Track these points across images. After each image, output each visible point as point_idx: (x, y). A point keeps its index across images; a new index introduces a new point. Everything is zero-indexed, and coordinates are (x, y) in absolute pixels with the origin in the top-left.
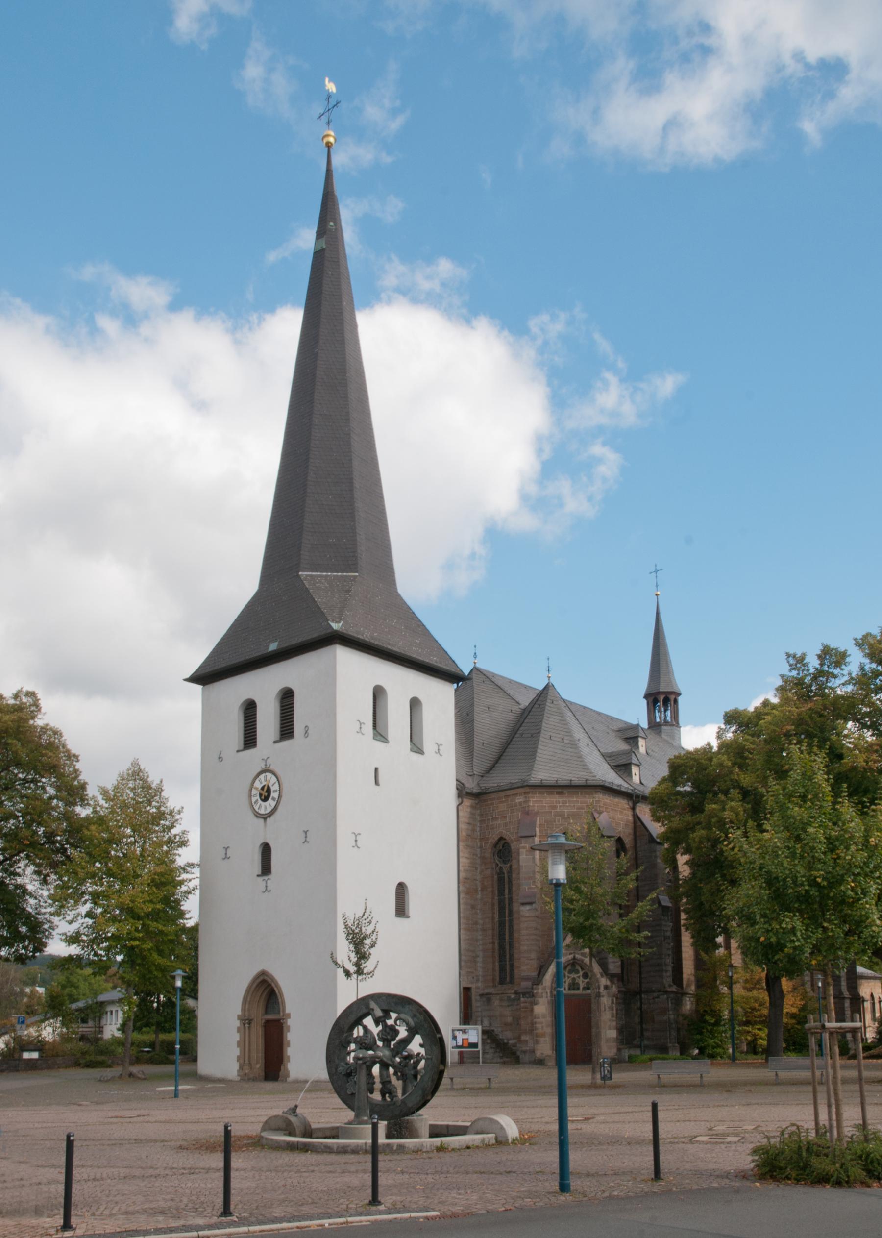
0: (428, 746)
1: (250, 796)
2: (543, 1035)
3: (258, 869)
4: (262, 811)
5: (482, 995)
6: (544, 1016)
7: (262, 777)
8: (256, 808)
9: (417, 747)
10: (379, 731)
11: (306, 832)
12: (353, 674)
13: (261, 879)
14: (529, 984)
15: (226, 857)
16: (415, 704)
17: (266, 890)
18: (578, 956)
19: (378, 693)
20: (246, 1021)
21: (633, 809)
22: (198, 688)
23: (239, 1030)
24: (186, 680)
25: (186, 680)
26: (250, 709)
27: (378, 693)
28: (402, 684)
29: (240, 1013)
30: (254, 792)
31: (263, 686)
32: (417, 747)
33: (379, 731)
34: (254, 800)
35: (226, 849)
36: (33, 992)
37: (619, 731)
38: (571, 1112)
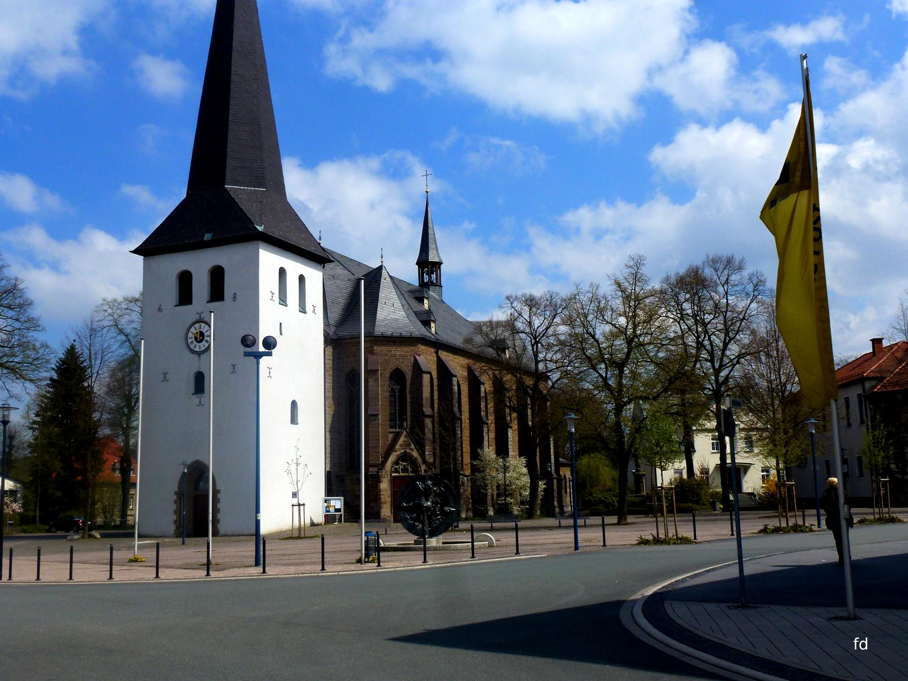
0: (309, 308)
1: (187, 338)
2: (385, 503)
3: (192, 389)
4: (197, 349)
5: (337, 477)
6: (386, 490)
7: (197, 325)
8: (192, 347)
9: (303, 310)
10: (283, 300)
11: (234, 366)
12: (270, 261)
13: (195, 396)
14: (376, 469)
15: (165, 380)
16: (302, 279)
17: (200, 404)
18: (408, 451)
19: (282, 271)
20: (180, 495)
21: (437, 353)
22: (140, 258)
23: (175, 502)
24: (134, 252)
25: (134, 252)
26: (185, 279)
27: (282, 271)
28: (295, 267)
29: (176, 490)
30: (190, 335)
31: (200, 264)
32: (303, 310)
33: (283, 300)
34: (190, 341)
35: (165, 374)
36: (434, 485)
37: (410, 292)
38: (579, 535)
